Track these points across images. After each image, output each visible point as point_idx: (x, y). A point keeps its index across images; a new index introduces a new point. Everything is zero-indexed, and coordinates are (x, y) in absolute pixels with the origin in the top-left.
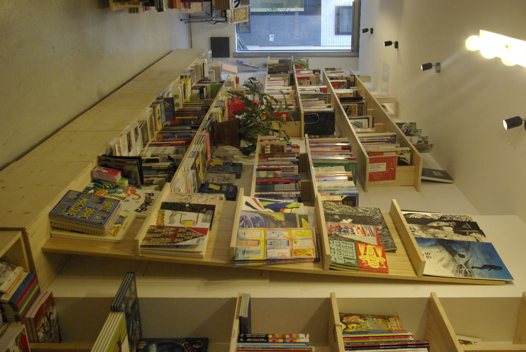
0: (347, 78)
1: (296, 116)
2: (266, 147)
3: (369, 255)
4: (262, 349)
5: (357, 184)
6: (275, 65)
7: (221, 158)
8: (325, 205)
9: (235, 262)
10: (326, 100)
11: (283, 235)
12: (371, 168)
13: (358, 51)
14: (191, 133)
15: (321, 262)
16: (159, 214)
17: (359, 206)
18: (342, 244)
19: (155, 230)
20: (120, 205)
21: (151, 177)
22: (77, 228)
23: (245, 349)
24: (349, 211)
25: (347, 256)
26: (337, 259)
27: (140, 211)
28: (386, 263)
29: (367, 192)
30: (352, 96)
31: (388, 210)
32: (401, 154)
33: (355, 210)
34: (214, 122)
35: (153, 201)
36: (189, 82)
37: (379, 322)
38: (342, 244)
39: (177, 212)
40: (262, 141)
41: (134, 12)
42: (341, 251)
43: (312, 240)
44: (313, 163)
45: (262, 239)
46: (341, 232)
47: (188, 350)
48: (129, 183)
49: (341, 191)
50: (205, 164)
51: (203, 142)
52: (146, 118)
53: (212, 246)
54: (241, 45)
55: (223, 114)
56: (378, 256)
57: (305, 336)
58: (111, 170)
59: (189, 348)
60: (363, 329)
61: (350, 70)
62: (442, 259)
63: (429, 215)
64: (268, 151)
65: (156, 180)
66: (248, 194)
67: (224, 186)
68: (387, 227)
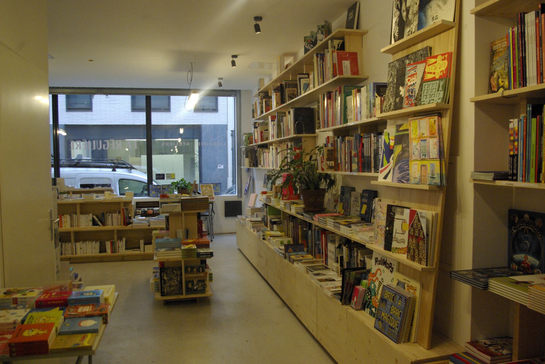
0: (262, 99)
1: (297, 141)
2: (328, 164)
3: (435, 70)
4: (524, 160)
5: (362, 86)
6: (250, 161)
7: (336, 205)
8: (386, 110)
9: (442, 185)
10: (282, 116)
11: (416, 145)
12: (347, 73)
13: (235, 91)
14: (315, 230)
15: (441, 112)
16: (395, 252)
17: (386, 82)
18: (425, 94)
19: (411, 255)
20: (387, 285)
21: (357, 261)
22: (408, 323)
23: (524, 174)
24: (391, 90)
25: (436, 88)
26: (439, 97)
27: (393, 268)
28: (442, 55)
29: (368, 76)
30: (279, 94)
31: (390, 56)
32: (335, 48)
33: (390, 84)
34: (304, 211)
35: (383, 258)
36: (269, 233)
37: (497, 59)
38: (425, 94)
39: (394, 236)
40: (323, 169)
41: (212, 277)
42: (431, 94)
43: (421, 120)
44: (344, 123)
45: (420, 163)
46: (412, 96)
47: (520, 227)
48: (365, 279)
49: (371, 98)
50: (343, 217)
51: (324, 219)
52: (304, 267)
53: (426, 206)
54: (230, 191)
55: (297, 203)
56: (436, 62)
57: (511, 123)
58: (354, 294)
59: (518, 226)
60: (504, 73)
61: (254, 97)
62: (439, 6)
63: (395, 19)
64: (332, 163)
65: (360, 257)
66: (376, 178)
67: (363, 201)
68: (407, 56)
